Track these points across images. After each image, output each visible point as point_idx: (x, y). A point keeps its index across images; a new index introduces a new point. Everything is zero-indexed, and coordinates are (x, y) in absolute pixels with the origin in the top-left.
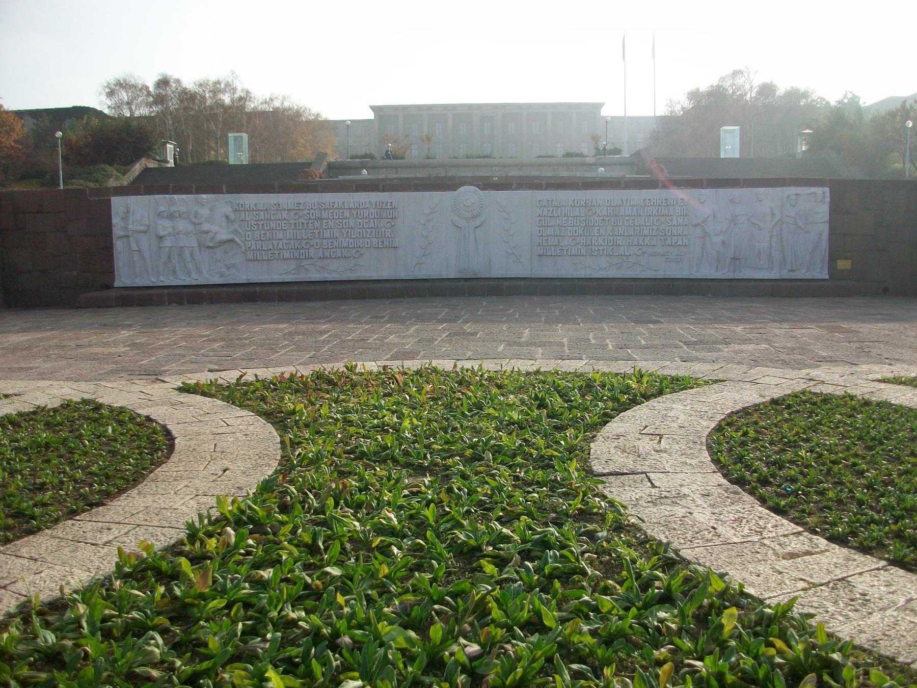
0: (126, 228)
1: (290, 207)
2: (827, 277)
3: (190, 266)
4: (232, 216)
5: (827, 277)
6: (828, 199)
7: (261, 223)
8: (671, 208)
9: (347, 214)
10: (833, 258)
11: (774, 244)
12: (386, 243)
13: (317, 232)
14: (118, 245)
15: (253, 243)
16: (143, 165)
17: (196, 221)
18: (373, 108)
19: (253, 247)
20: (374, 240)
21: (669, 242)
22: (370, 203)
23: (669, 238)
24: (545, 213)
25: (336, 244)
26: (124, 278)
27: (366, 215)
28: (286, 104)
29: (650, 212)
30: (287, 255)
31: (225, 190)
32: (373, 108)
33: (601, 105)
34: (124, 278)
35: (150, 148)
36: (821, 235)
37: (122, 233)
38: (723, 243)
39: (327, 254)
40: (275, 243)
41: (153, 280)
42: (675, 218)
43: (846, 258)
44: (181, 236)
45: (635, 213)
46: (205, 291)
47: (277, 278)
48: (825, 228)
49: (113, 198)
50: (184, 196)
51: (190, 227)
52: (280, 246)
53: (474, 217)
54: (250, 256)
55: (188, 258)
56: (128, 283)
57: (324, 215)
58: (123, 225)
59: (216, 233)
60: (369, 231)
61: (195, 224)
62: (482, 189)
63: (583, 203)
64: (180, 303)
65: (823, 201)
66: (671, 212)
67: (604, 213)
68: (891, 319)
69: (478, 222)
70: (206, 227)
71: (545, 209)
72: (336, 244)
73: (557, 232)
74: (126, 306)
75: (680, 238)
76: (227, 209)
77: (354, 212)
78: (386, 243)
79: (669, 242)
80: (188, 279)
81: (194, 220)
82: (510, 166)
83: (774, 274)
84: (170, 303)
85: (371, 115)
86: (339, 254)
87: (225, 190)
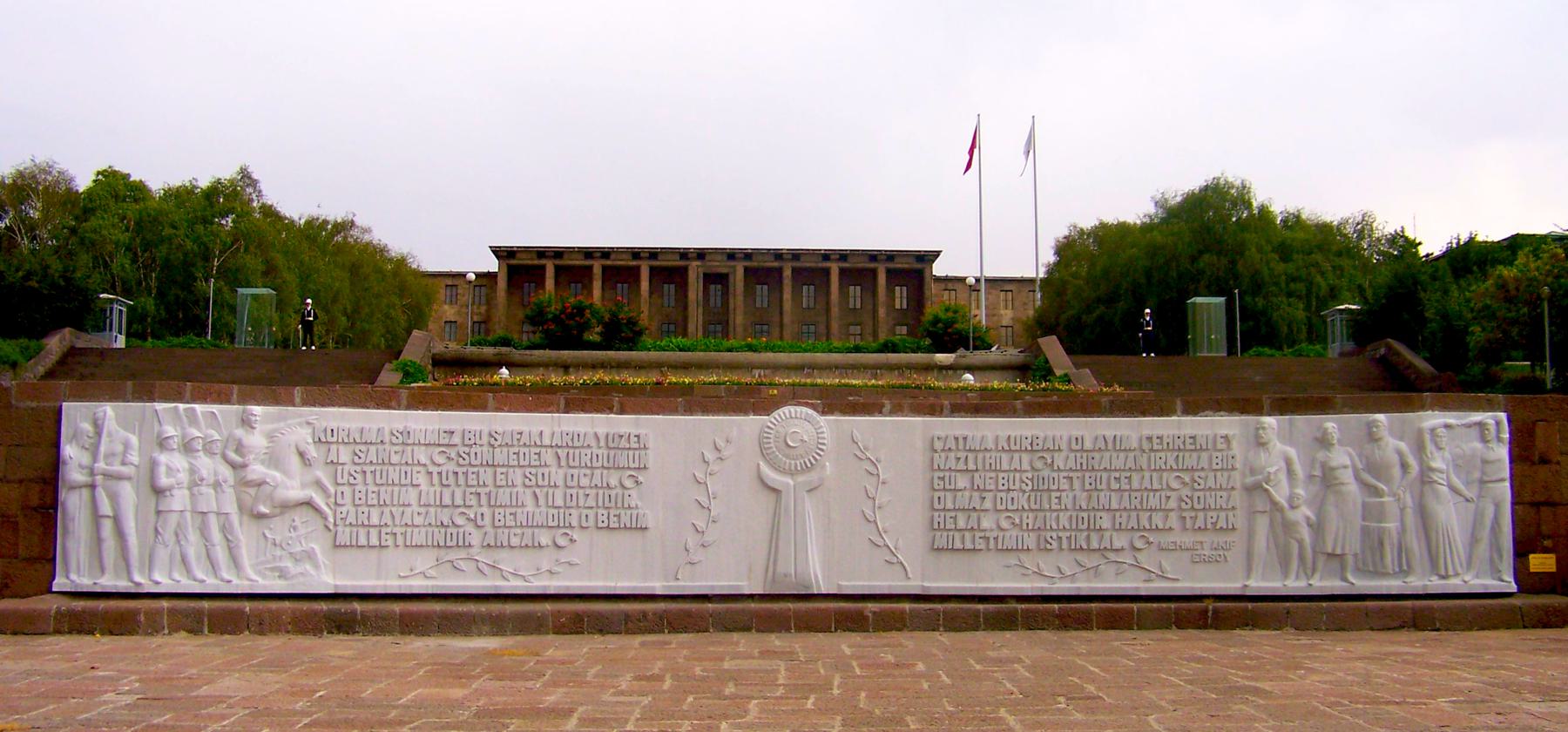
1: (433, 439)
2: (1513, 588)
3: (221, 553)
4: (312, 452)
6: (1506, 436)
7: (368, 469)
9: (548, 456)
10: (1522, 549)
14: (74, 504)
16: (67, 344)
17: (238, 459)
18: (497, 252)
20: (601, 511)
22: (596, 436)
28: (367, 238)
29: (1160, 463)
30: (419, 538)
31: (298, 400)
32: (497, 252)
33: (937, 254)
34: (78, 571)
35: (1416, 282)
39: (503, 536)
40: (397, 511)
43: (1546, 550)
44: (204, 489)
45: (1130, 464)
46: (247, 606)
50: (215, 408)
51: (226, 472)
53: (807, 469)
56: (85, 582)
57: (500, 456)
59: (275, 487)
61: (234, 466)
62: (823, 413)
63: (1026, 444)
66: (1204, 463)
67: (1071, 464)
70: (257, 470)
73: (976, 504)
74: (79, 632)
75: (1223, 515)
76: (303, 436)
78: (625, 519)
79: (1200, 523)
80: (236, 581)
81: (233, 456)
84: (174, 629)
85: (492, 265)
87: (298, 400)
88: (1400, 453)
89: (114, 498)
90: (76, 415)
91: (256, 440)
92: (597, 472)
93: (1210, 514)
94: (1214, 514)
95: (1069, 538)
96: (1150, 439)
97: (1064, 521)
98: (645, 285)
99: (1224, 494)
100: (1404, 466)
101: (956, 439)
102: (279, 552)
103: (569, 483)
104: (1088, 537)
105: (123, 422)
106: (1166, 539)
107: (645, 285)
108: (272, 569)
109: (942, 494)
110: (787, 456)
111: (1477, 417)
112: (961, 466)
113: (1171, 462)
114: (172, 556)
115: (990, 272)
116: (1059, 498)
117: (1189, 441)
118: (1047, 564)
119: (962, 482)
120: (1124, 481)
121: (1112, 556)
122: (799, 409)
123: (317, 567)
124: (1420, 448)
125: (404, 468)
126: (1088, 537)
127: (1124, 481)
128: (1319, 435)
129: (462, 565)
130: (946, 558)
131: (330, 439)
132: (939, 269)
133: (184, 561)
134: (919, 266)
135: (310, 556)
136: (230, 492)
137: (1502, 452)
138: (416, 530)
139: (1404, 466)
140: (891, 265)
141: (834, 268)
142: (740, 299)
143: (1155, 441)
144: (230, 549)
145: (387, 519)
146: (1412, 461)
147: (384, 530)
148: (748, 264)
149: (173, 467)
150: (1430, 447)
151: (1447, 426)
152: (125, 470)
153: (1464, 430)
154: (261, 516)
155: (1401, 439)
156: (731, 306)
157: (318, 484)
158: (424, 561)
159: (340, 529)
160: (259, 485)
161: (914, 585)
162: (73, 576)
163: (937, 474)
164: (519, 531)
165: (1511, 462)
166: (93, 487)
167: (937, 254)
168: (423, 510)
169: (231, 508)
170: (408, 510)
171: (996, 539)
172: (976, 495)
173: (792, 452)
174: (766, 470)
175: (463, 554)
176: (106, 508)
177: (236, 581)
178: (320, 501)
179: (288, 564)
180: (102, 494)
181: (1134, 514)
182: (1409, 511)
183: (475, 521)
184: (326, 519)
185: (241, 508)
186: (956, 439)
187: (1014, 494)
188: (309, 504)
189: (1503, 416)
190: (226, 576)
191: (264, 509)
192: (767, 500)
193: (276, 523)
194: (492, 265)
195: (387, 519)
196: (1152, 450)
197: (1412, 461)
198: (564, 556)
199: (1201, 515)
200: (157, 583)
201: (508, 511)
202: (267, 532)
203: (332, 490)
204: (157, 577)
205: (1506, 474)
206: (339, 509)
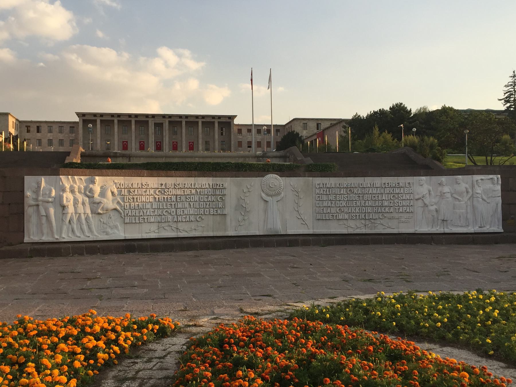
0: (36, 200)
3: (85, 227)
5: (502, 231)
6: (500, 182)
8: (402, 189)
11: (469, 211)
12: (219, 212)
13: (173, 203)
14: (29, 211)
15: (130, 211)
18: (78, 114)
19: (130, 214)
21: (401, 210)
23: (401, 208)
24: (322, 192)
25: (186, 212)
26: (33, 234)
27: (206, 192)
30: (152, 220)
32: (78, 114)
33: (235, 116)
34: (33, 234)
36: (497, 204)
37: (32, 202)
38: (437, 211)
39: (180, 219)
41: (56, 237)
42: (404, 195)
47: (145, 236)
48: (499, 200)
49: (26, 178)
52: (148, 213)
54: (127, 221)
55: (84, 222)
56: (35, 238)
58: (34, 197)
60: (208, 203)
61: (88, 197)
64: (81, 254)
65: (498, 183)
66: (402, 191)
68: (125, 176)
69: (279, 198)
71: (322, 190)
72: (186, 212)
73: (330, 204)
75: (408, 208)
77: (198, 191)
79: (401, 210)
80: (91, 236)
82: (248, 157)
83: (471, 229)
85: (77, 119)
86: (188, 219)
88: (466, 188)
89: (47, 210)
90: (29, 181)
91: (97, 189)
92: (210, 197)
93: (404, 208)
94: (405, 208)
95: (336, 216)
96: (385, 184)
97: (357, 210)
98: (133, 127)
99: (408, 201)
100: (467, 192)
101: (323, 184)
102: (105, 226)
103: (201, 200)
104: (365, 215)
105: (46, 182)
106: (392, 215)
107: (133, 127)
108: (104, 232)
109: (319, 202)
110: (270, 190)
111: (491, 176)
112: (325, 193)
113: (391, 191)
114: (68, 228)
115: (256, 123)
116: (356, 203)
117: (397, 184)
118: (352, 223)
119: (325, 198)
120: (376, 197)
121: (372, 221)
122: (273, 175)
123: (118, 230)
124: (473, 187)
125: (147, 196)
126: (365, 215)
127: (376, 197)
128: (439, 182)
129: (166, 228)
130: (320, 222)
131: (122, 187)
132: (236, 121)
133: (73, 231)
134: (229, 120)
135: (116, 227)
136: (87, 205)
137: (499, 188)
138: (151, 217)
139: (467, 192)
140: (219, 120)
141: (200, 121)
142: (167, 132)
143: (386, 184)
144: (88, 226)
145: (141, 214)
146: (470, 190)
147: (141, 218)
148: (170, 119)
149: (68, 197)
150: (476, 186)
151: (482, 179)
152: (50, 200)
153: (487, 181)
154: (99, 214)
155: (467, 183)
156: (164, 134)
157: (118, 203)
158: (154, 227)
159: (126, 218)
160: (98, 203)
161: (311, 232)
162: (32, 237)
163: (317, 196)
164: (185, 216)
165: (502, 191)
166: (38, 205)
167: (235, 116)
168: (153, 210)
169: (88, 211)
170: (148, 211)
171: (336, 216)
172: (330, 202)
173: (271, 189)
174: (263, 195)
175: (167, 224)
176: (43, 213)
177: (91, 236)
178: (118, 208)
179: (109, 230)
180: (41, 207)
181: (380, 208)
182: (469, 207)
183: (170, 213)
184: (121, 214)
185: (92, 212)
186: (323, 184)
187: (342, 202)
188: (115, 209)
189: (499, 176)
190: (88, 235)
191: (100, 211)
192: (262, 203)
193: (104, 216)
194: (77, 119)
195: (141, 214)
196: (385, 187)
197: (470, 190)
198: (199, 224)
199: (401, 208)
200: (64, 238)
201: (182, 210)
202: (101, 219)
203: (122, 203)
204: (63, 236)
205: (500, 194)
206: (125, 211)
